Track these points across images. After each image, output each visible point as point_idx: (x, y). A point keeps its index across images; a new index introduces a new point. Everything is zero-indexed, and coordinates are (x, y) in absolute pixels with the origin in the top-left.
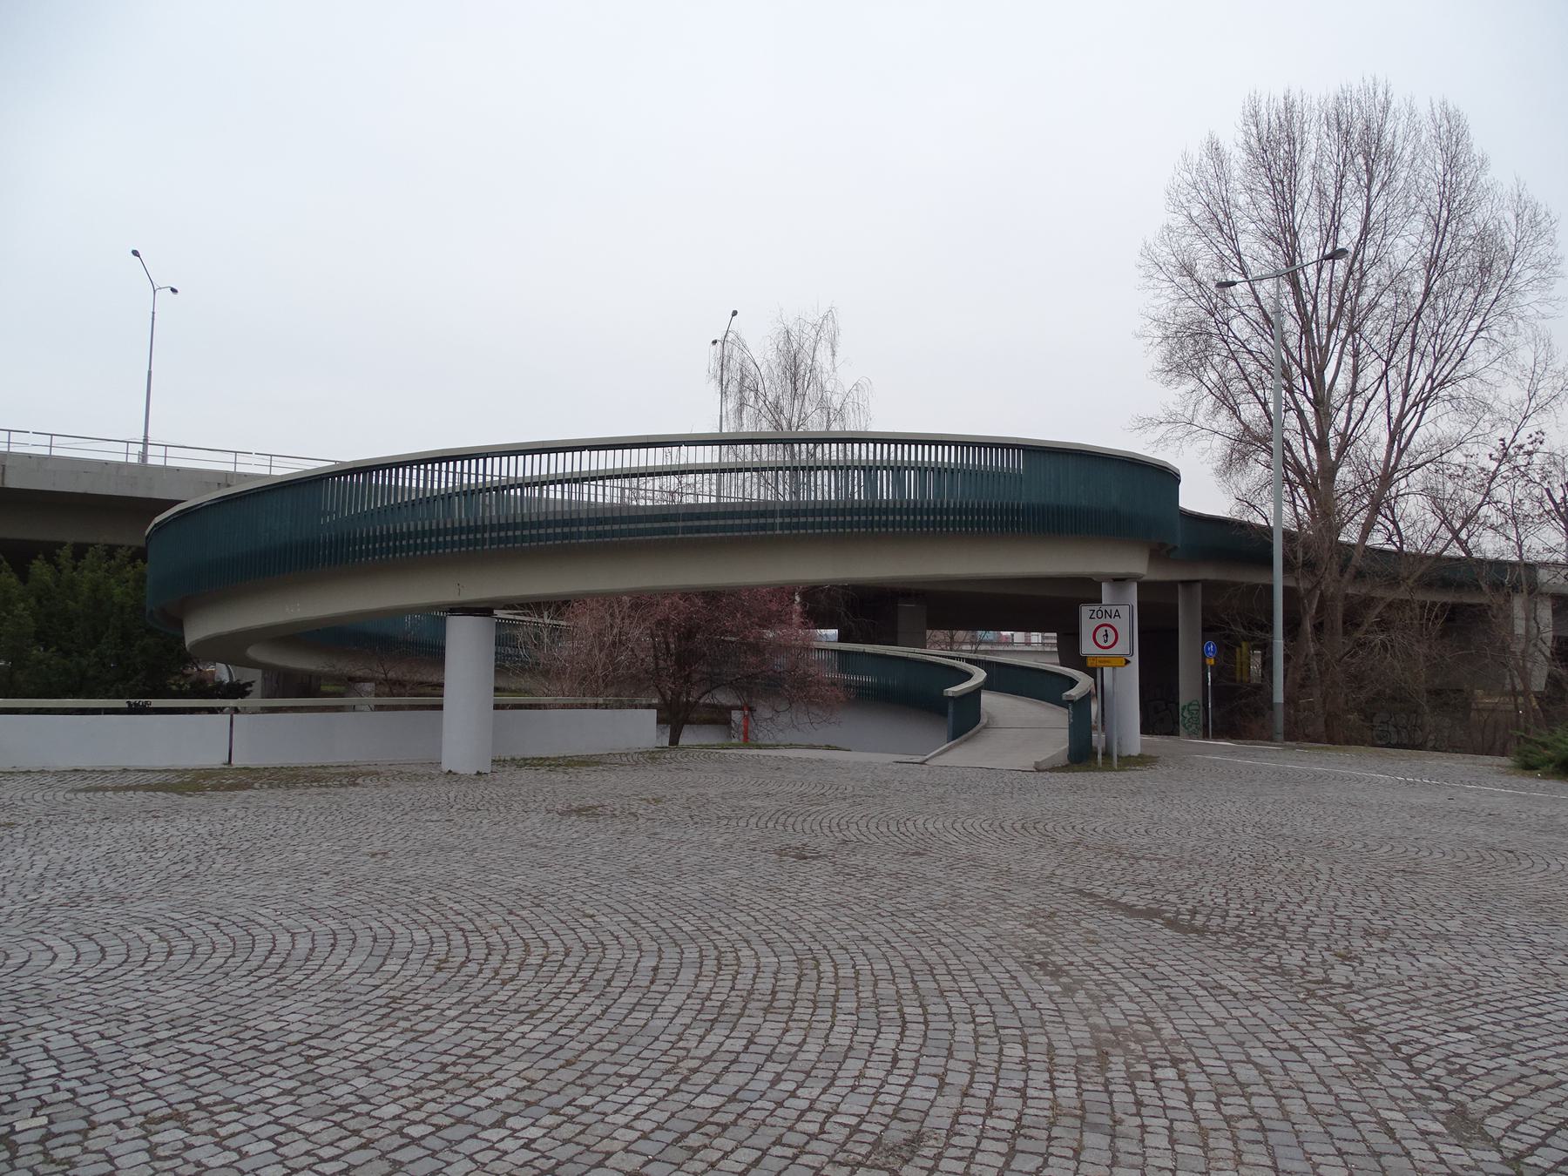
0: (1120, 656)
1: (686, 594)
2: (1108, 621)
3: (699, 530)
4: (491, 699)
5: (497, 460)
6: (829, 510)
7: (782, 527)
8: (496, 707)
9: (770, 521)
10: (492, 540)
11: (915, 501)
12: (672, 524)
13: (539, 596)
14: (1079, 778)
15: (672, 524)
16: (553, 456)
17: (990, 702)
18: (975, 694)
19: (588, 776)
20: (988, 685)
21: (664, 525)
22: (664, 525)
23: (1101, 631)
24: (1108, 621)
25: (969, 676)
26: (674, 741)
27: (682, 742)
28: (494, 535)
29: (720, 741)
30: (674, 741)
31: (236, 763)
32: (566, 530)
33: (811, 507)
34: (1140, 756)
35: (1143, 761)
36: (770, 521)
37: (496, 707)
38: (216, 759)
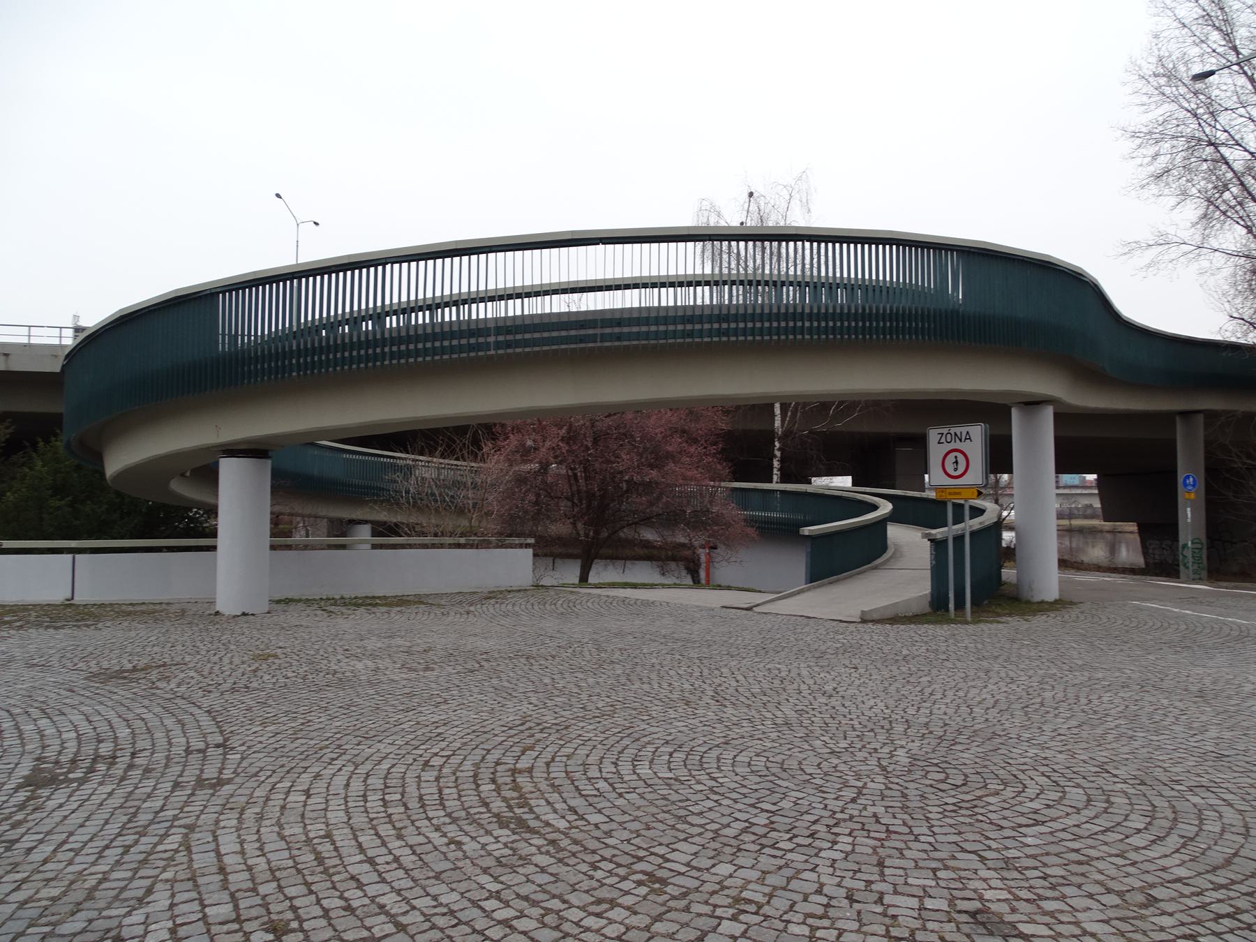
0: (970, 486)
1: (672, 405)
2: (958, 445)
3: (517, 344)
4: (267, 540)
5: (396, 266)
6: (666, 318)
7: (498, 345)
8: (273, 547)
9: (501, 338)
10: (392, 354)
11: (795, 306)
12: (590, 332)
13: (426, 420)
14: (941, 631)
15: (590, 332)
16: (474, 257)
17: (897, 533)
18: (881, 524)
19: (398, 618)
20: (894, 517)
21: (582, 332)
22: (582, 332)
23: (951, 458)
24: (958, 445)
25: (874, 507)
26: (584, 579)
27: (592, 579)
28: (395, 348)
29: (656, 578)
30: (584, 579)
31: (78, 599)
32: (473, 341)
33: (707, 312)
34: (1056, 602)
35: (1060, 604)
36: (501, 338)
37: (273, 547)
38: (58, 595)
